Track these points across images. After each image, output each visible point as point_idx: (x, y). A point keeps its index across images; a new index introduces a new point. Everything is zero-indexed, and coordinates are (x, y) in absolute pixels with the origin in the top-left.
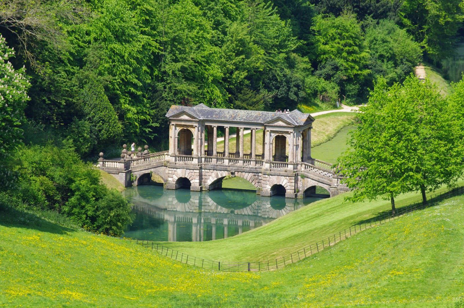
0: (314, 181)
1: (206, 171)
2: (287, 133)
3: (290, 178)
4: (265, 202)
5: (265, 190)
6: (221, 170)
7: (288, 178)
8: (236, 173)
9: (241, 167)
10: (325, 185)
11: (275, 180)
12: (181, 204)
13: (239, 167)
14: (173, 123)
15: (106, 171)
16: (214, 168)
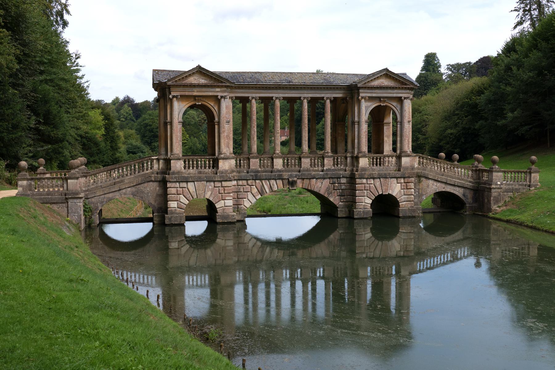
0: (439, 184)
1: (240, 183)
2: (400, 100)
3: (406, 180)
4: (362, 230)
5: (362, 207)
6: (269, 179)
7: (402, 180)
8: (299, 181)
9: (307, 170)
10: (457, 189)
11: (378, 187)
12: (196, 251)
13: (304, 171)
14: (173, 94)
15: (36, 199)
16: (256, 175)
